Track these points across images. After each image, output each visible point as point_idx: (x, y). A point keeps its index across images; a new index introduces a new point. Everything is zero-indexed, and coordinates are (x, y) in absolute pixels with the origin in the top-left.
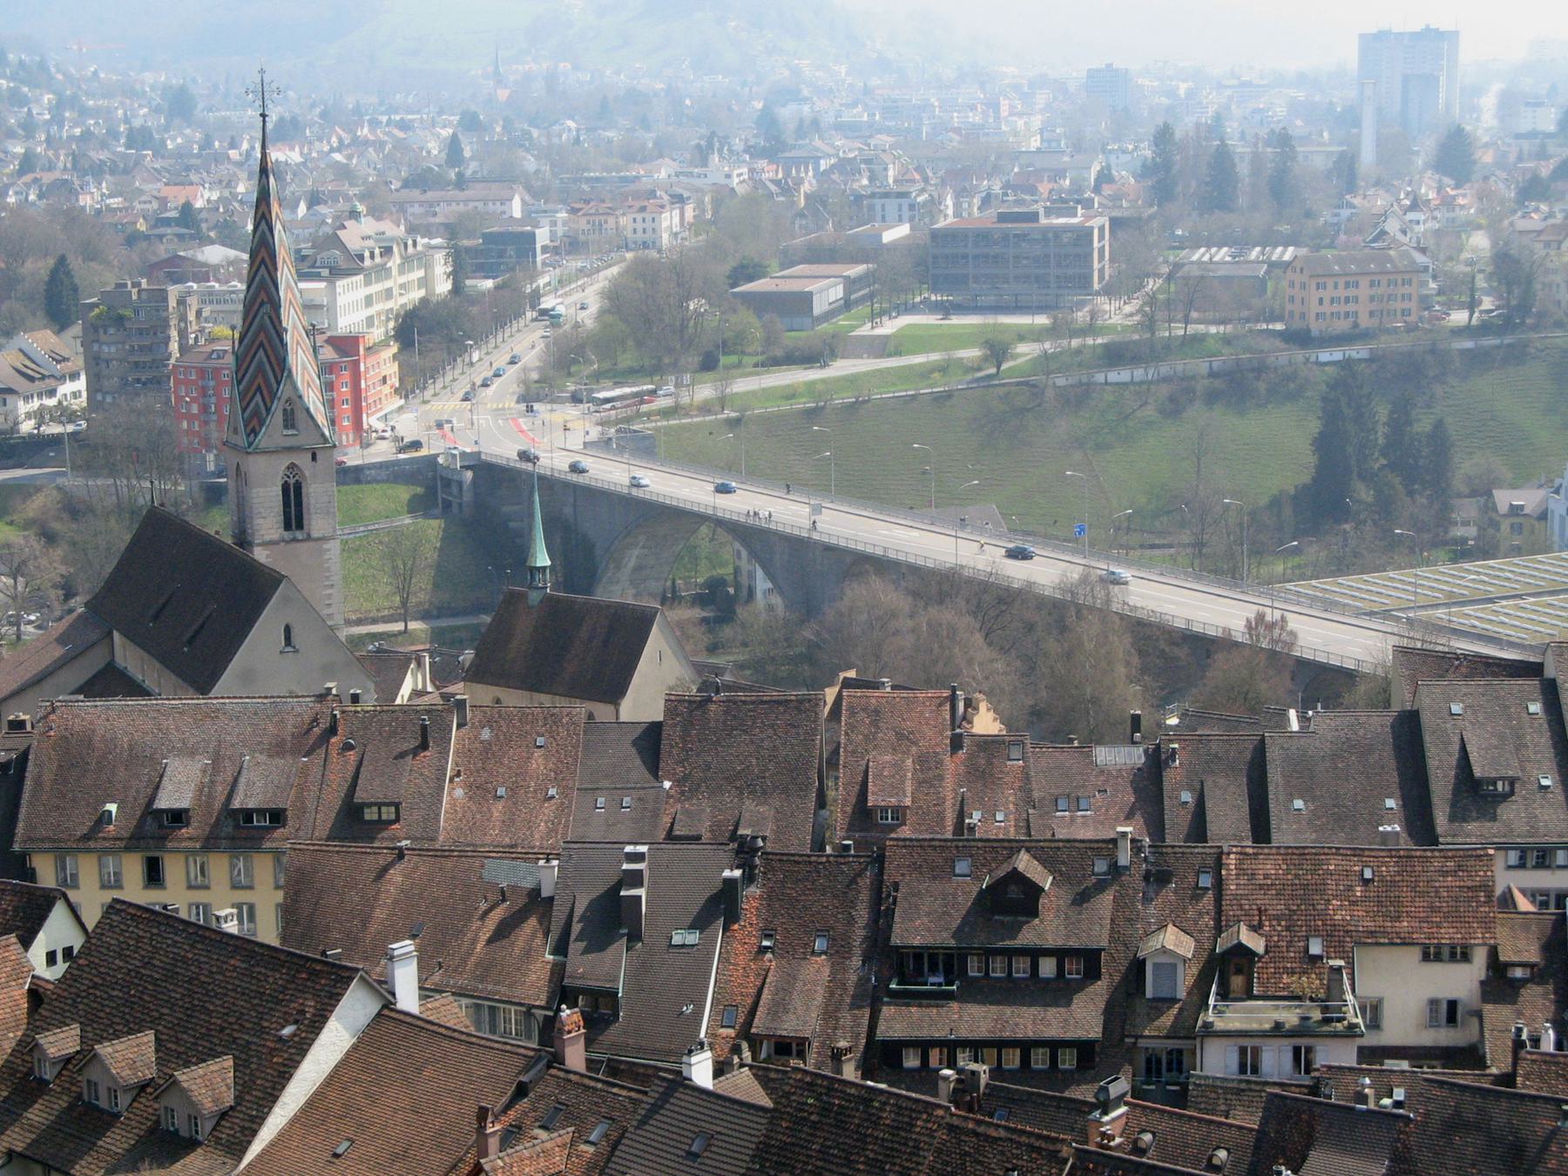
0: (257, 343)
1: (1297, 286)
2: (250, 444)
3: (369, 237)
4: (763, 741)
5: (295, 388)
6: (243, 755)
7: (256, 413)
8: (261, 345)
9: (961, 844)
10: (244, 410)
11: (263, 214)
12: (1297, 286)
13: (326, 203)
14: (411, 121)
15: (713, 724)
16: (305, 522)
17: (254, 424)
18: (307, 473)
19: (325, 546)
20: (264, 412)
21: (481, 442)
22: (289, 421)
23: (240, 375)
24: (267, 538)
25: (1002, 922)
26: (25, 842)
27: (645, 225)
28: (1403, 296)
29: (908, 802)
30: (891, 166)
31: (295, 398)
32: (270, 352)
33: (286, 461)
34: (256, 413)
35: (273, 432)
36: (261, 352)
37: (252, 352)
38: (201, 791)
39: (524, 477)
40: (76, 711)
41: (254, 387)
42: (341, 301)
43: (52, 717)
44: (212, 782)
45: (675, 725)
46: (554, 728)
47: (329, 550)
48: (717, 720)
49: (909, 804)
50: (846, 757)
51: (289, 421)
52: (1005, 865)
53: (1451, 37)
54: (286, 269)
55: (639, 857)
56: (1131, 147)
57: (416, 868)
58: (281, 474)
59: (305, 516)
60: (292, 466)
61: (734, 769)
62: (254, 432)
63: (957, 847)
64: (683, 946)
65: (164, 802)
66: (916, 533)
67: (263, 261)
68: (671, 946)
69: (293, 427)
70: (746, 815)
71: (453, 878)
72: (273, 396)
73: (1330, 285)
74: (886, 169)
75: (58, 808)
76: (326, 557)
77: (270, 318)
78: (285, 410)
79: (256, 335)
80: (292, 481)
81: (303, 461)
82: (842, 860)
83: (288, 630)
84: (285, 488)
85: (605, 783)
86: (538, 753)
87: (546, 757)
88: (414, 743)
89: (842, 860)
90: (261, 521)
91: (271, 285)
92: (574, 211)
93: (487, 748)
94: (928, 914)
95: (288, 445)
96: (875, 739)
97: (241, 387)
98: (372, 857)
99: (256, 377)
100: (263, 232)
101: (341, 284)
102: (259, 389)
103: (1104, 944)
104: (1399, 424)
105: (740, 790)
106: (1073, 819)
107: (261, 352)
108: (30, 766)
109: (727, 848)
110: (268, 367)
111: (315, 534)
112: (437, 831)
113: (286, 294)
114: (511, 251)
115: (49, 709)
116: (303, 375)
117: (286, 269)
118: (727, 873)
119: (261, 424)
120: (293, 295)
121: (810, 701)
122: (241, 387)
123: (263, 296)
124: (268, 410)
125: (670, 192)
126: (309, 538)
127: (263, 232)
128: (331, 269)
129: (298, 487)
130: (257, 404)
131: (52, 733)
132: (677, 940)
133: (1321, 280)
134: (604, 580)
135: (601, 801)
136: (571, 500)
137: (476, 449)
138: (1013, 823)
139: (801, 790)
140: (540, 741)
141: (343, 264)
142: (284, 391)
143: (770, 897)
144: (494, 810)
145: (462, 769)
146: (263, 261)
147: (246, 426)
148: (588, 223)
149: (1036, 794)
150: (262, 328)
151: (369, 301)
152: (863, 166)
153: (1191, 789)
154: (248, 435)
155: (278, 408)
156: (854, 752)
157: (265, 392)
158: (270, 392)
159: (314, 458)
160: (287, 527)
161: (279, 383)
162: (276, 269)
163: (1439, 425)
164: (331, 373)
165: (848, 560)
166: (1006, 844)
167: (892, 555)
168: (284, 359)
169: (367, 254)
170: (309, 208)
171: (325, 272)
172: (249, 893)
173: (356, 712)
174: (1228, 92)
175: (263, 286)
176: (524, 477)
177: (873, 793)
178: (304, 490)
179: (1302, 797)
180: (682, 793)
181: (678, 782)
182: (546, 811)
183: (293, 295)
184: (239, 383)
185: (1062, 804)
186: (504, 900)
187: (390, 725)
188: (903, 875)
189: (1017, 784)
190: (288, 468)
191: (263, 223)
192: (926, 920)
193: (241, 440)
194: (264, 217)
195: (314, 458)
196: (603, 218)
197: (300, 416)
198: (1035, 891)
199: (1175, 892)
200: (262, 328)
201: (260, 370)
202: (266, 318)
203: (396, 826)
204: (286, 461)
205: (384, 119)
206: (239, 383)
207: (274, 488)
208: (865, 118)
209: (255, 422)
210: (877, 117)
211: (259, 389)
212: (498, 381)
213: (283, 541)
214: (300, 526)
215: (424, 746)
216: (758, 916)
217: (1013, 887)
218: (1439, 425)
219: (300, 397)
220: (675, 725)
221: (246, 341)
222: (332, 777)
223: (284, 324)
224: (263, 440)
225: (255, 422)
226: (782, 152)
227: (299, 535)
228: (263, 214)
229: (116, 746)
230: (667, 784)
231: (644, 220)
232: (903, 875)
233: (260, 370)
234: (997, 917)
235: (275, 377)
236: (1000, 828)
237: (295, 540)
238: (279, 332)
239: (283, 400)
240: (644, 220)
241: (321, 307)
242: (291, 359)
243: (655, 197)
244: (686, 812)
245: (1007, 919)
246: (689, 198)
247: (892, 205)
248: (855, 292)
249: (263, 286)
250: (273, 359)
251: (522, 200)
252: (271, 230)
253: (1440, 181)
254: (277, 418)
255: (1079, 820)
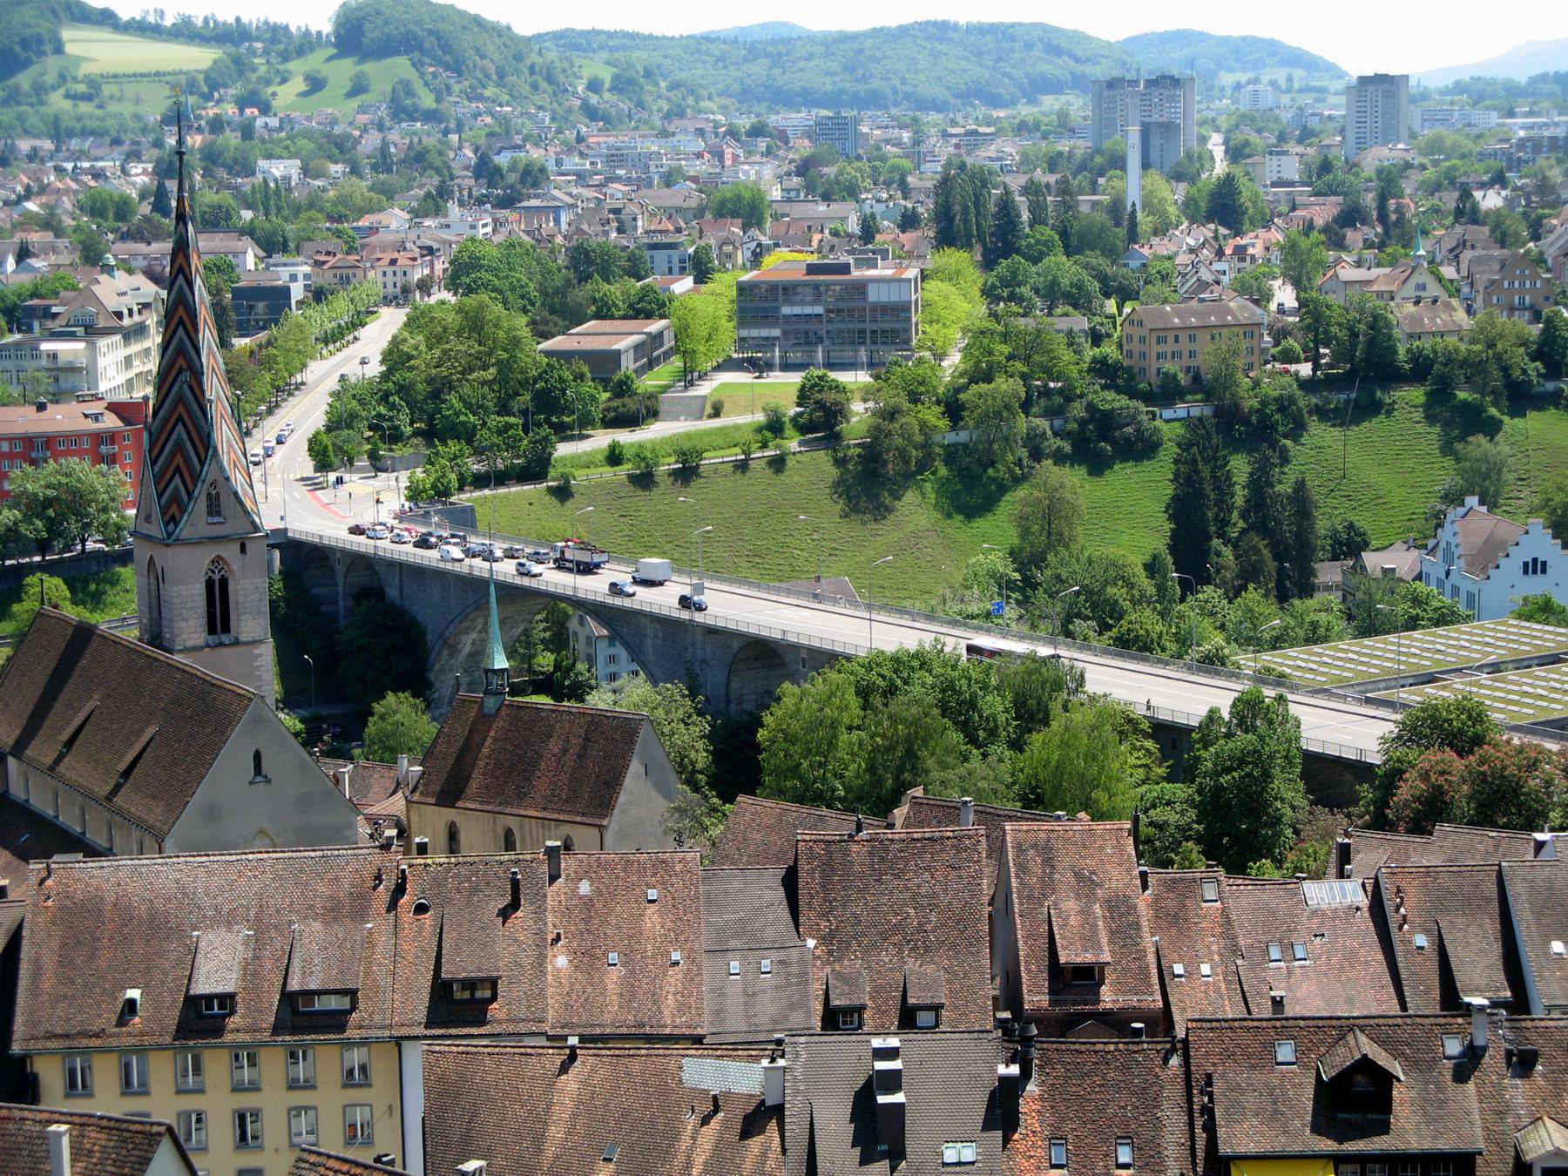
0: (175, 416)
1: (1136, 340)
2: (169, 535)
3: (124, 294)
4: (919, 886)
5: (222, 469)
6: (290, 923)
7: (175, 498)
8: (180, 419)
9: (1278, 1024)
10: (160, 496)
11: (181, 266)
12: (1136, 340)
13: (36, 256)
14: (102, 169)
15: (857, 868)
16: (233, 623)
17: (173, 511)
18: (235, 567)
19: (256, 651)
20: (185, 498)
21: (287, 519)
22: (214, 507)
23: (155, 453)
24: (189, 644)
25: (1349, 1122)
26: (27, 1040)
27: (394, 279)
28: (1173, 353)
29: (1106, 957)
30: (640, 217)
31: (221, 480)
32: (191, 428)
33: (207, 554)
34: (175, 498)
35: (195, 522)
36: (180, 427)
37: (169, 428)
38: (245, 969)
39: (338, 555)
40: (76, 874)
41: (172, 468)
42: (102, 362)
43: (49, 882)
44: (256, 957)
45: (813, 870)
46: (667, 877)
47: (261, 655)
48: (862, 864)
49: (1109, 959)
50: (1021, 904)
51: (214, 507)
52: (1341, 1050)
53: (1406, 77)
54: (207, 331)
55: (891, 1054)
56: (885, 196)
57: (593, 1069)
58: (205, 569)
59: (233, 617)
60: (218, 560)
61: (889, 922)
62: (174, 520)
63: (1275, 1027)
64: (959, 1164)
65: (201, 987)
66: (806, 613)
67: (181, 322)
68: (945, 1165)
69: (219, 513)
70: (912, 980)
71: (645, 1083)
72: (196, 478)
73: (1171, 339)
74: (635, 219)
75: (65, 997)
76: (258, 664)
77: (190, 387)
78: (209, 494)
79: (174, 408)
80: (217, 577)
81: (230, 552)
82: (1135, 1048)
83: (257, 757)
84: (210, 584)
85: (735, 943)
86: (652, 908)
87: (661, 914)
88: (507, 900)
89: (1135, 1048)
90: (183, 624)
91: (191, 350)
92: (318, 264)
93: (588, 904)
94: (1257, 1115)
95: (213, 535)
96: (1052, 881)
97: (157, 468)
98: (534, 1059)
99: (175, 455)
100: (181, 289)
101: (103, 343)
102: (178, 470)
103: (1481, 1145)
104: (1259, 484)
105: (899, 947)
106: (1290, 972)
107: (180, 427)
108: (25, 943)
109: (990, 1036)
110: (188, 445)
111: (244, 638)
112: (544, 1011)
113: (208, 359)
114: (261, 306)
115: (44, 873)
116: (229, 453)
117: (207, 331)
118: (1002, 1070)
119: (183, 511)
120: (216, 361)
121: (970, 837)
122: (157, 468)
123: (181, 362)
124: (190, 495)
125: (419, 243)
126: (237, 642)
127: (181, 289)
128: (86, 327)
129: (224, 583)
130: (176, 488)
131: (50, 903)
132: (950, 1155)
133: (1162, 334)
134: (437, 668)
135: (735, 966)
136: (397, 581)
137: (281, 525)
138: (1221, 977)
139: (971, 945)
140: (653, 894)
141: (102, 323)
142: (209, 472)
143: (1050, 1096)
144: (608, 981)
145: (561, 931)
146: (181, 322)
147: (163, 513)
148: (335, 275)
149: (1242, 942)
150: (181, 399)
151: (128, 361)
152: (611, 216)
153: (1427, 932)
154: (167, 524)
155: (201, 492)
156: (1029, 897)
157: (186, 474)
158: (191, 473)
159: (243, 549)
160: (212, 630)
161: (202, 464)
162: (197, 331)
163: (1300, 485)
164: (113, 443)
165: (736, 644)
166: (1334, 1023)
167: (792, 638)
168: (209, 435)
169: (126, 312)
170: (18, 262)
171: (80, 331)
172: (309, 1093)
173: (426, 865)
174: (954, 141)
175: (181, 351)
176: (338, 555)
177: (1064, 948)
178: (231, 587)
179: (1559, 938)
180: (830, 953)
181: (825, 939)
182: (672, 980)
183: (216, 361)
184: (154, 463)
185: (1275, 953)
186: (716, 1109)
187: (470, 881)
188: (1214, 1064)
189: (1218, 930)
190: (213, 562)
191: (181, 278)
192: (1255, 1122)
193: (156, 529)
194: (181, 270)
195: (243, 549)
196: (350, 272)
197: (226, 501)
198: (1387, 1079)
199: (1544, 1076)
200: (181, 399)
201: (179, 447)
202: (185, 387)
203: (495, 1005)
204: (207, 554)
205: (69, 166)
206: (154, 463)
207: (198, 585)
208: (588, 167)
209: (174, 509)
210: (599, 166)
211: (178, 470)
212: (280, 452)
213: (208, 646)
214: (226, 629)
215: (514, 905)
216: (1041, 1122)
217: (1359, 1078)
218: (1300, 485)
219: (227, 479)
220: (813, 870)
221: (162, 412)
222: (405, 946)
223: (208, 395)
224: (185, 529)
225: (174, 509)
226: (520, 201)
227: (225, 639)
228: (181, 266)
229: (132, 918)
230: (811, 943)
231: (395, 273)
232: (1214, 1064)
233: (179, 447)
234: (1341, 1115)
235: (199, 457)
236: (1207, 983)
237: (221, 645)
238: (202, 404)
239: (208, 482)
240: (395, 273)
241: (81, 369)
242: (216, 436)
243: (405, 249)
244: (840, 976)
245: (1354, 1117)
246: (438, 250)
247: (661, 256)
248: (655, 350)
249: (181, 351)
250: (194, 434)
251: (256, 256)
252: (190, 285)
253: (1216, 231)
254: (201, 505)
255: (1298, 971)
